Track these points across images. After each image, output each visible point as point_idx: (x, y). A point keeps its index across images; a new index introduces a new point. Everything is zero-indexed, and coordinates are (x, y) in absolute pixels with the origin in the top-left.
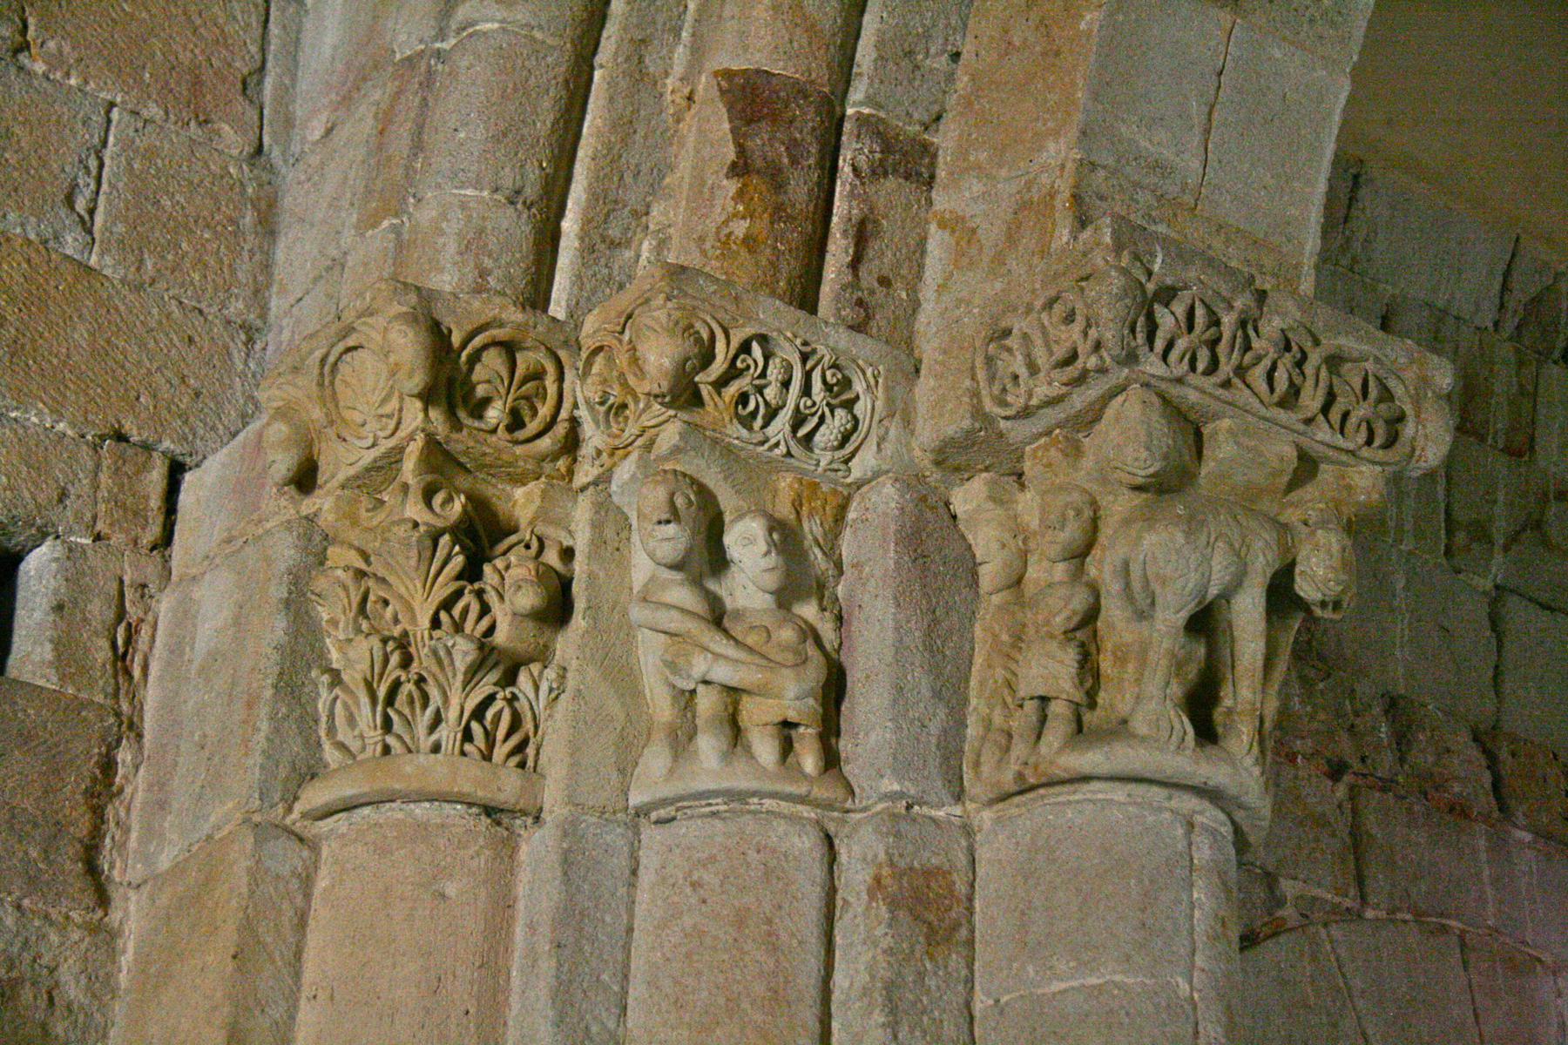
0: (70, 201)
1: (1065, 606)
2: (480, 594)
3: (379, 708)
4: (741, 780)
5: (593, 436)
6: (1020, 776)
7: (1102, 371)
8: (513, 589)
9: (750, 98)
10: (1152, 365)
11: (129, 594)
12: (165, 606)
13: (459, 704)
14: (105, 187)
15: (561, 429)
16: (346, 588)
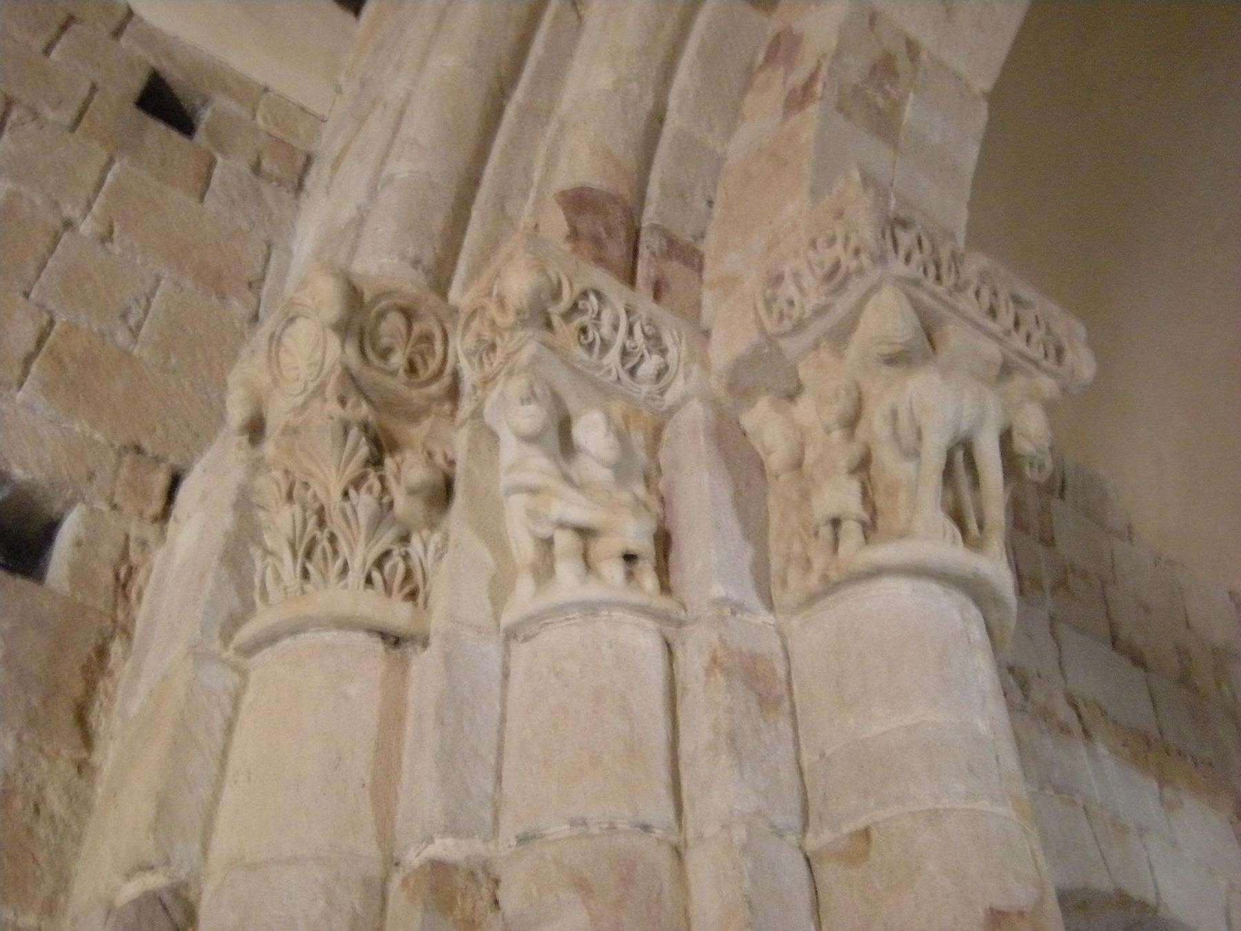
0: (124, 316)
1: (845, 456)
2: (382, 479)
3: (300, 561)
4: (593, 591)
5: (469, 376)
6: (825, 577)
7: (860, 272)
8: (410, 471)
9: (579, 202)
10: (897, 267)
11: (133, 546)
12: (158, 557)
13: (360, 556)
14: (150, 315)
15: (446, 380)
16: (278, 485)
